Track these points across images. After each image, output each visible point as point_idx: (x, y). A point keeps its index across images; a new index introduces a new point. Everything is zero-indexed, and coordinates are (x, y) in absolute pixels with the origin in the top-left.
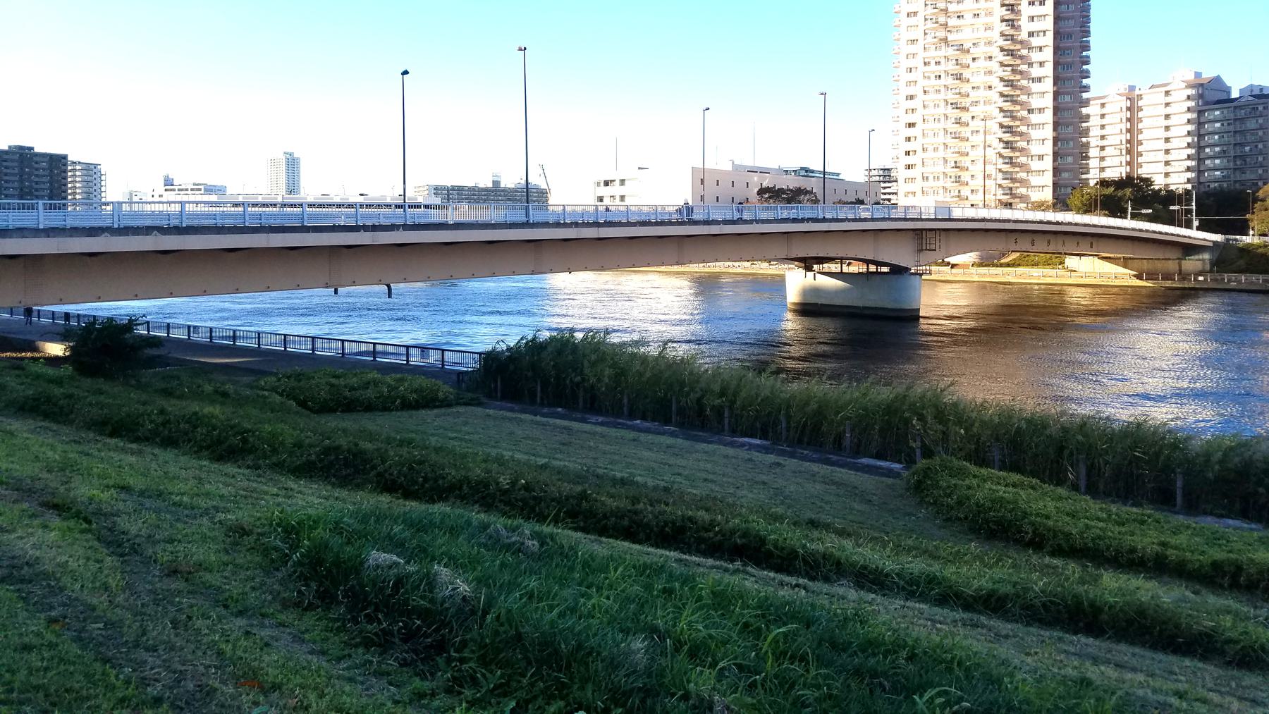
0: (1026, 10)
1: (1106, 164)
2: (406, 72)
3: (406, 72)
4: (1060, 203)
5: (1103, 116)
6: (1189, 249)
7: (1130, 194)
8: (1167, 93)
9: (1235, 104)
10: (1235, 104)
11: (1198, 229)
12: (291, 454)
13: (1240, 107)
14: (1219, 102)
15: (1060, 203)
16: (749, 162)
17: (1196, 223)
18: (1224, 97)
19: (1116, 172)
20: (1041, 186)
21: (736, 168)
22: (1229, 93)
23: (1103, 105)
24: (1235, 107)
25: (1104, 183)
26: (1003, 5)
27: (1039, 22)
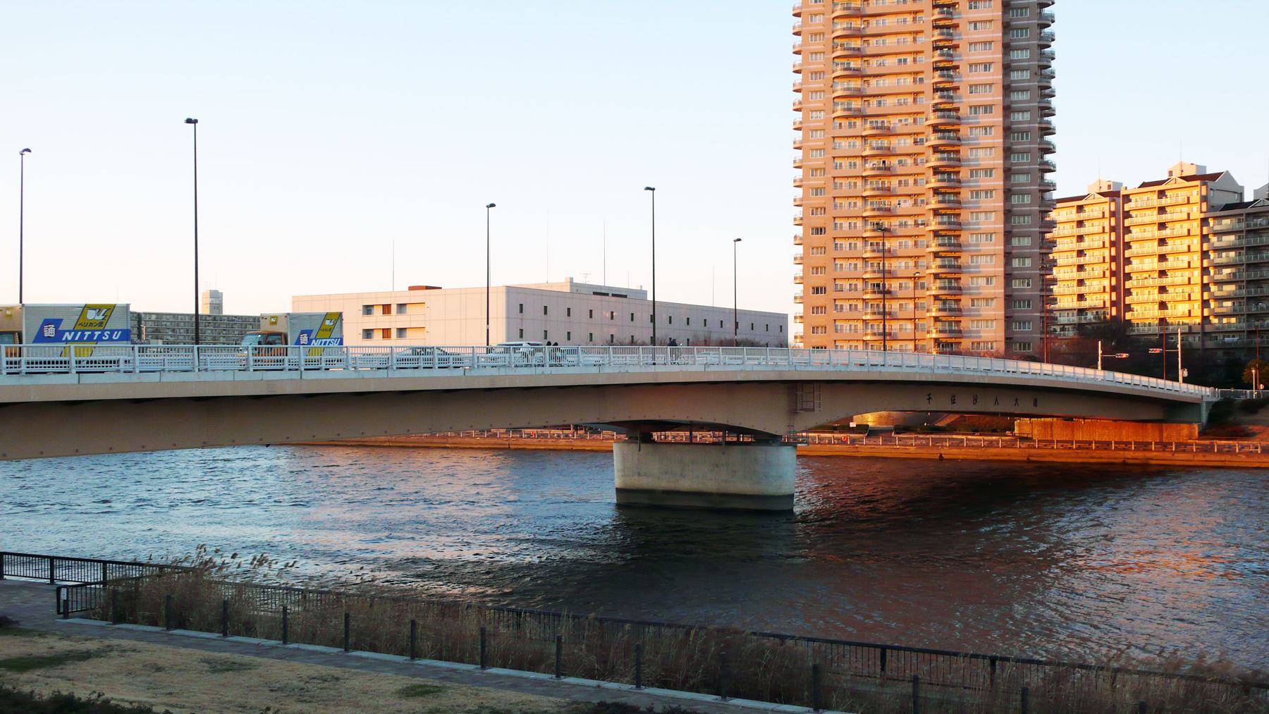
0: (965, 14)
1: (1078, 287)
2: (493, 205)
3: (493, 205)
4: (1014, 348)
5: (1080, 224)
6: (1173, 409)
7: (1109, 336)
8: (1162, 194)
9: (1249, 210)
10: (1249, 210)
11: (1186, 380)
12: (1063, 329)
13: (1256, 215)
14: (1228, 207)
15: (1014, 348)
16: (597, 280)
17: (1182, 373)
18: (1234, 199)
19: (1098, 296)
20: (987, 325)
21: (577, 289)
22: (1241, 195)
23: (1080, 209)
24: (1248, 215)
25: (1190, 423)
26: (935, 7)
27: (980, 29)
